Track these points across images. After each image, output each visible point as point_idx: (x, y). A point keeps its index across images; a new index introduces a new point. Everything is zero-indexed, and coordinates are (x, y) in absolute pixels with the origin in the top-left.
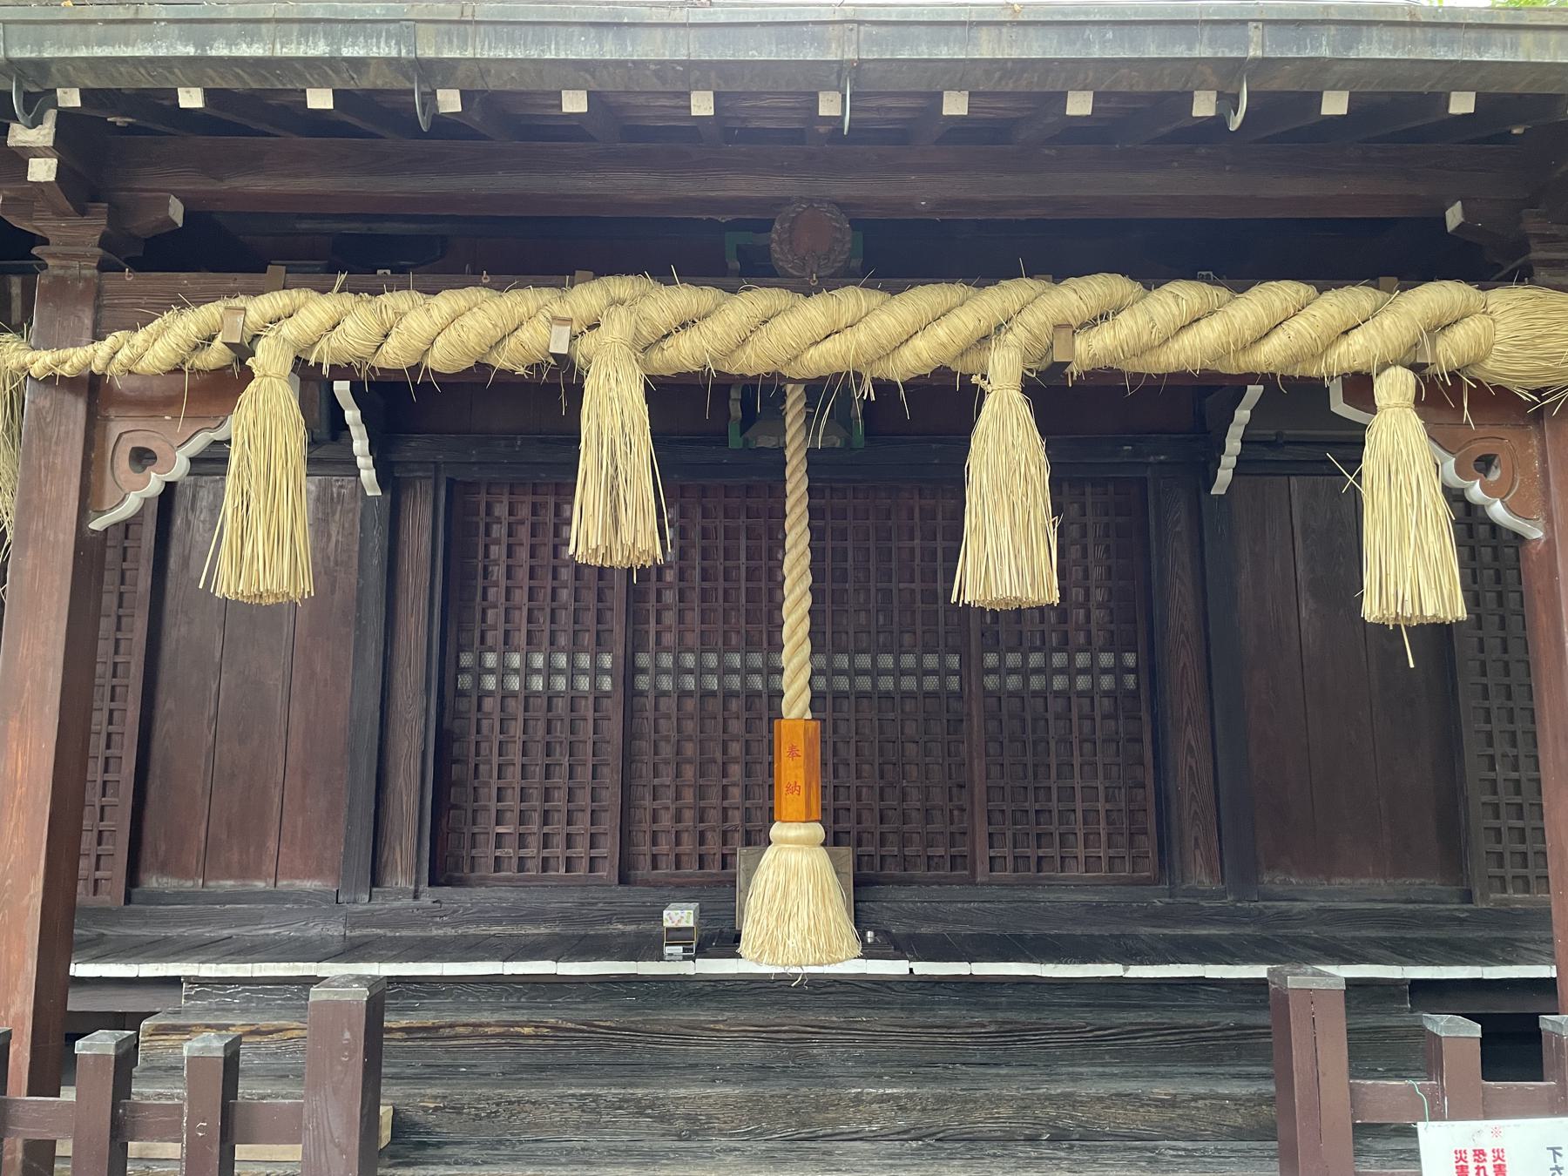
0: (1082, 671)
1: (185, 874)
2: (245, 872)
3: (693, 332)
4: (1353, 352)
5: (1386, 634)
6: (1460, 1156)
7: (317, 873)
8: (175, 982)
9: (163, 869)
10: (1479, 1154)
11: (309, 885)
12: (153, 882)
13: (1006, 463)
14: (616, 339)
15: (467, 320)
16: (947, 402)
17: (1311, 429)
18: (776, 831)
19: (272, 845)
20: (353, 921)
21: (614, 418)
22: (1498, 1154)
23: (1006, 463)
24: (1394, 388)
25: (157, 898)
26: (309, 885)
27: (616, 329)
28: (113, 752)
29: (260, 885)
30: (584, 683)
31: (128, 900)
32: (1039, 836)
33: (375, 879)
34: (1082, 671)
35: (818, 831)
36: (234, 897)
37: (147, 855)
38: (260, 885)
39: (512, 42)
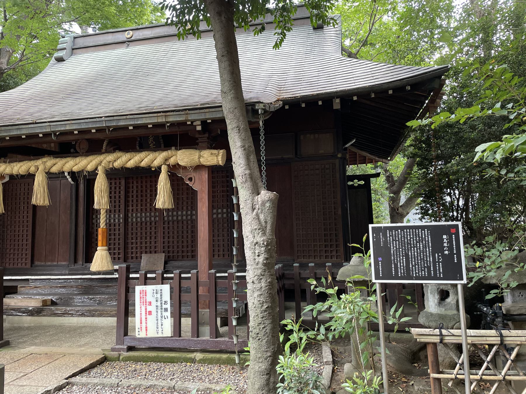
0: (220, 213)
1: (42, 262)
2: (53, 261)
3: (55, 166)
4: (156, 163)
5: (160, 211)
6: (141, 291)
7: (64, 261)
8: (28, 280)
9: (38, 261)
10: (143, 291)
11: (64, 263)
12: (37, 263)
13: (101, 185)
14: (40, 168)
15: (22, 167)
16: (93, 174)
17: (150, 175)
18: (98, 248)
19: (57, 256)
20: (70, 270)
21: (40, 181)
22: (146, 291)
23: (101, 185)
24: (164, 169)
25: (37, 266)
26: (64, 263)
27: (41, 168)
28: (338, 243)
29: (55, 263)
30: (220, 216)
31: (31, 266)
32: (320, 256)
33: (76, 262)
34: (220, 213)
35: (106, 248)
36: (50, 266)
37: (35, 258)
38: (55, 263)
39: (6, 132)
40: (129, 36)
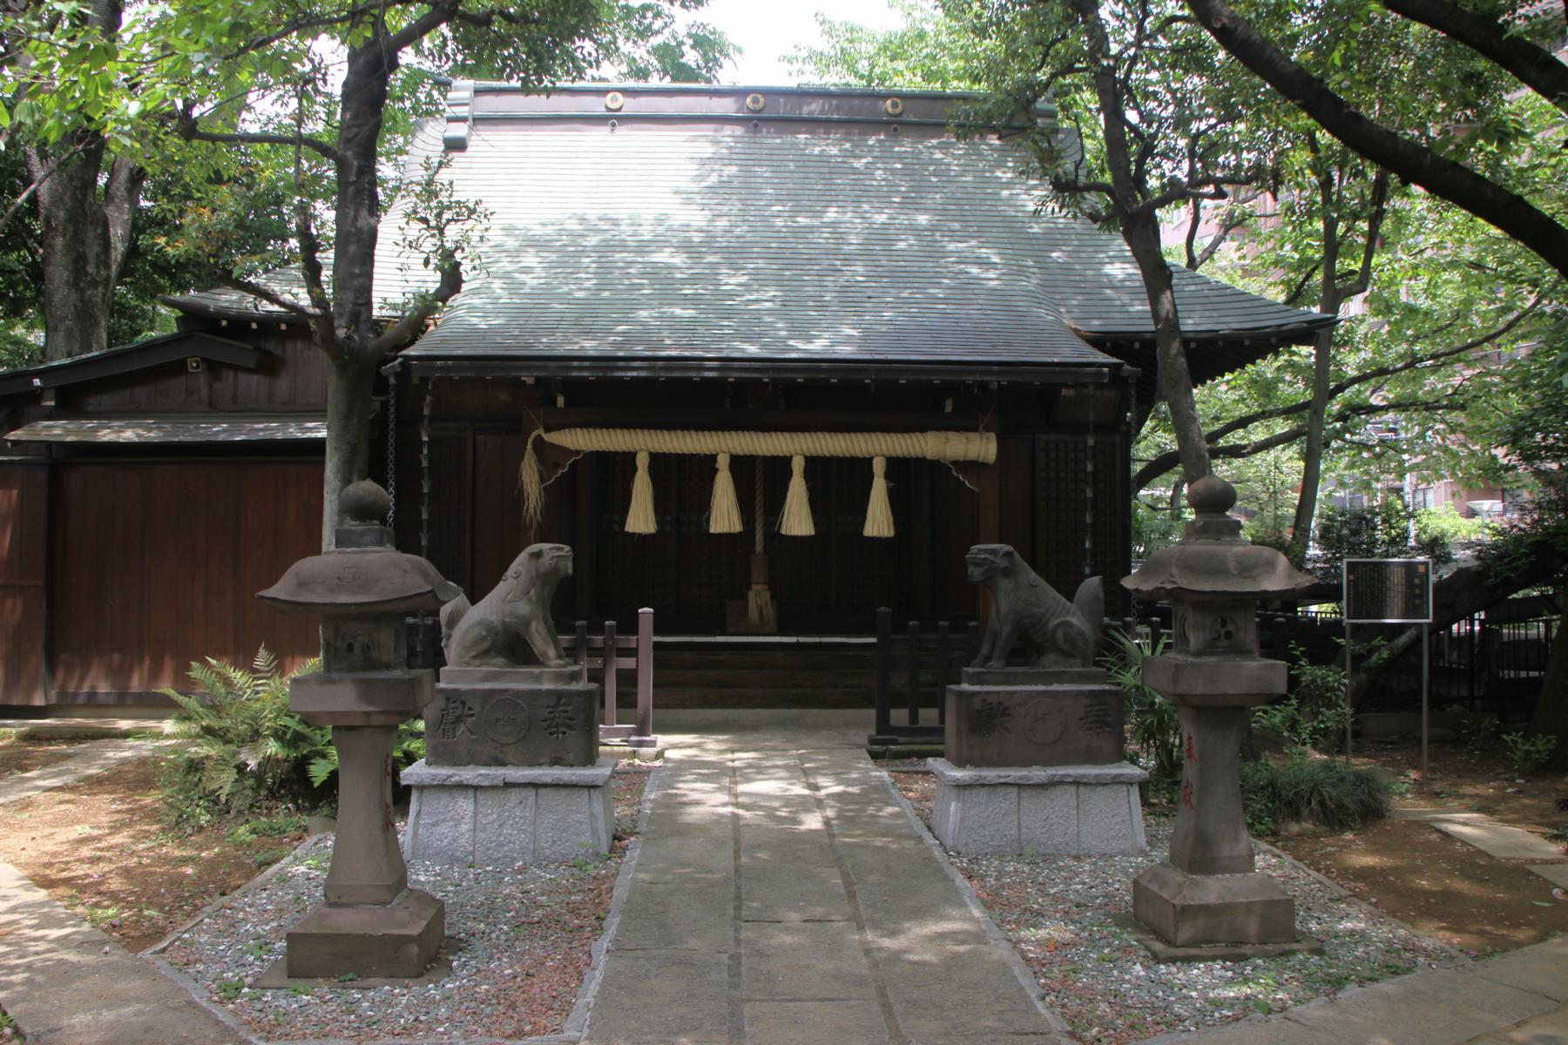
23: (797, 491)
40: (614, 106)
